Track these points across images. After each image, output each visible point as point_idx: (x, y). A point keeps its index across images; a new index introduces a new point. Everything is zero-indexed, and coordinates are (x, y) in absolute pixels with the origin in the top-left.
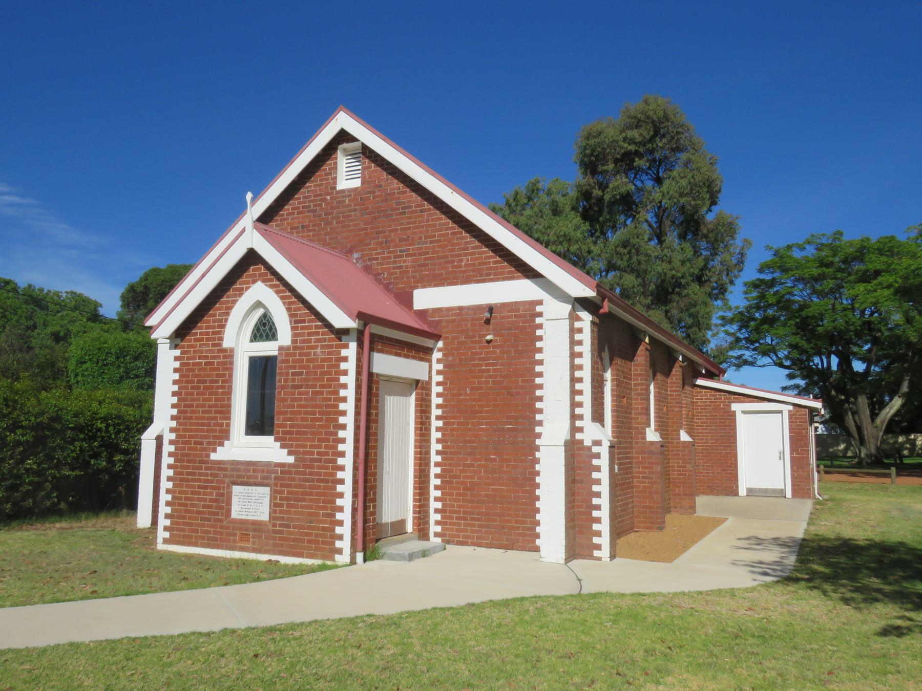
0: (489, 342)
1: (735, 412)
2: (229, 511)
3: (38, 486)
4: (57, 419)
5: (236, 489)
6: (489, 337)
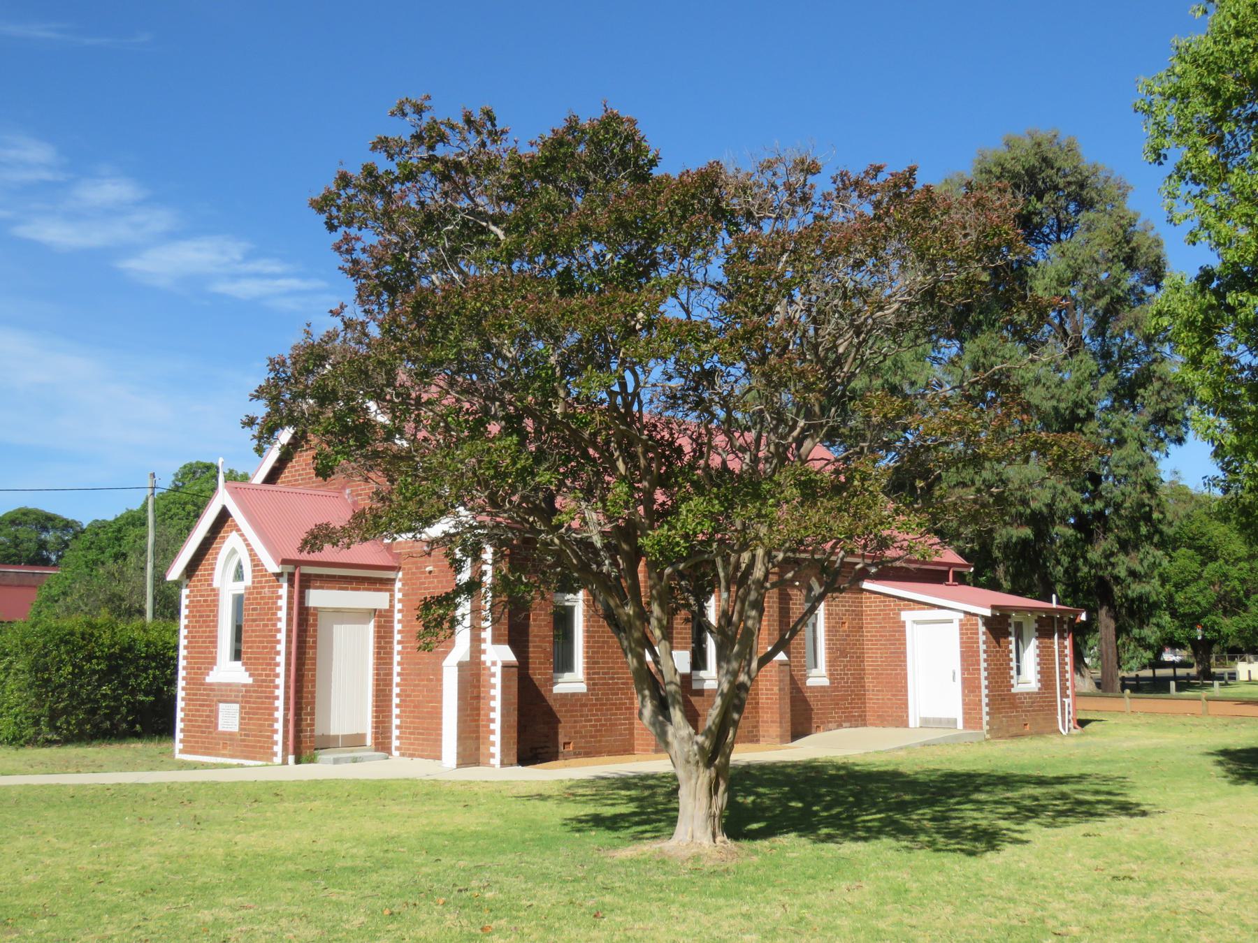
0: (430, 572)
1: (904, 622)
2: (216, 725)
3: (115, 710)
4: (130, 649)
5: (222, 706)
6: (428, 569)
